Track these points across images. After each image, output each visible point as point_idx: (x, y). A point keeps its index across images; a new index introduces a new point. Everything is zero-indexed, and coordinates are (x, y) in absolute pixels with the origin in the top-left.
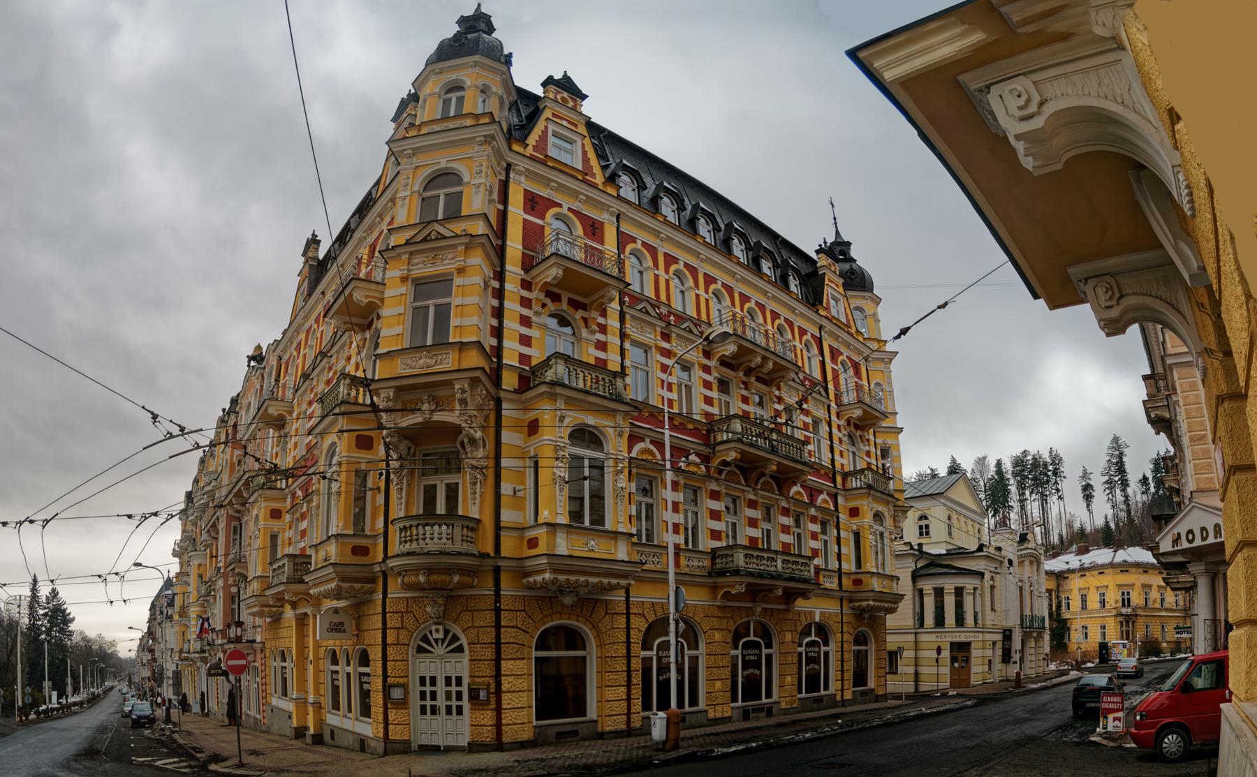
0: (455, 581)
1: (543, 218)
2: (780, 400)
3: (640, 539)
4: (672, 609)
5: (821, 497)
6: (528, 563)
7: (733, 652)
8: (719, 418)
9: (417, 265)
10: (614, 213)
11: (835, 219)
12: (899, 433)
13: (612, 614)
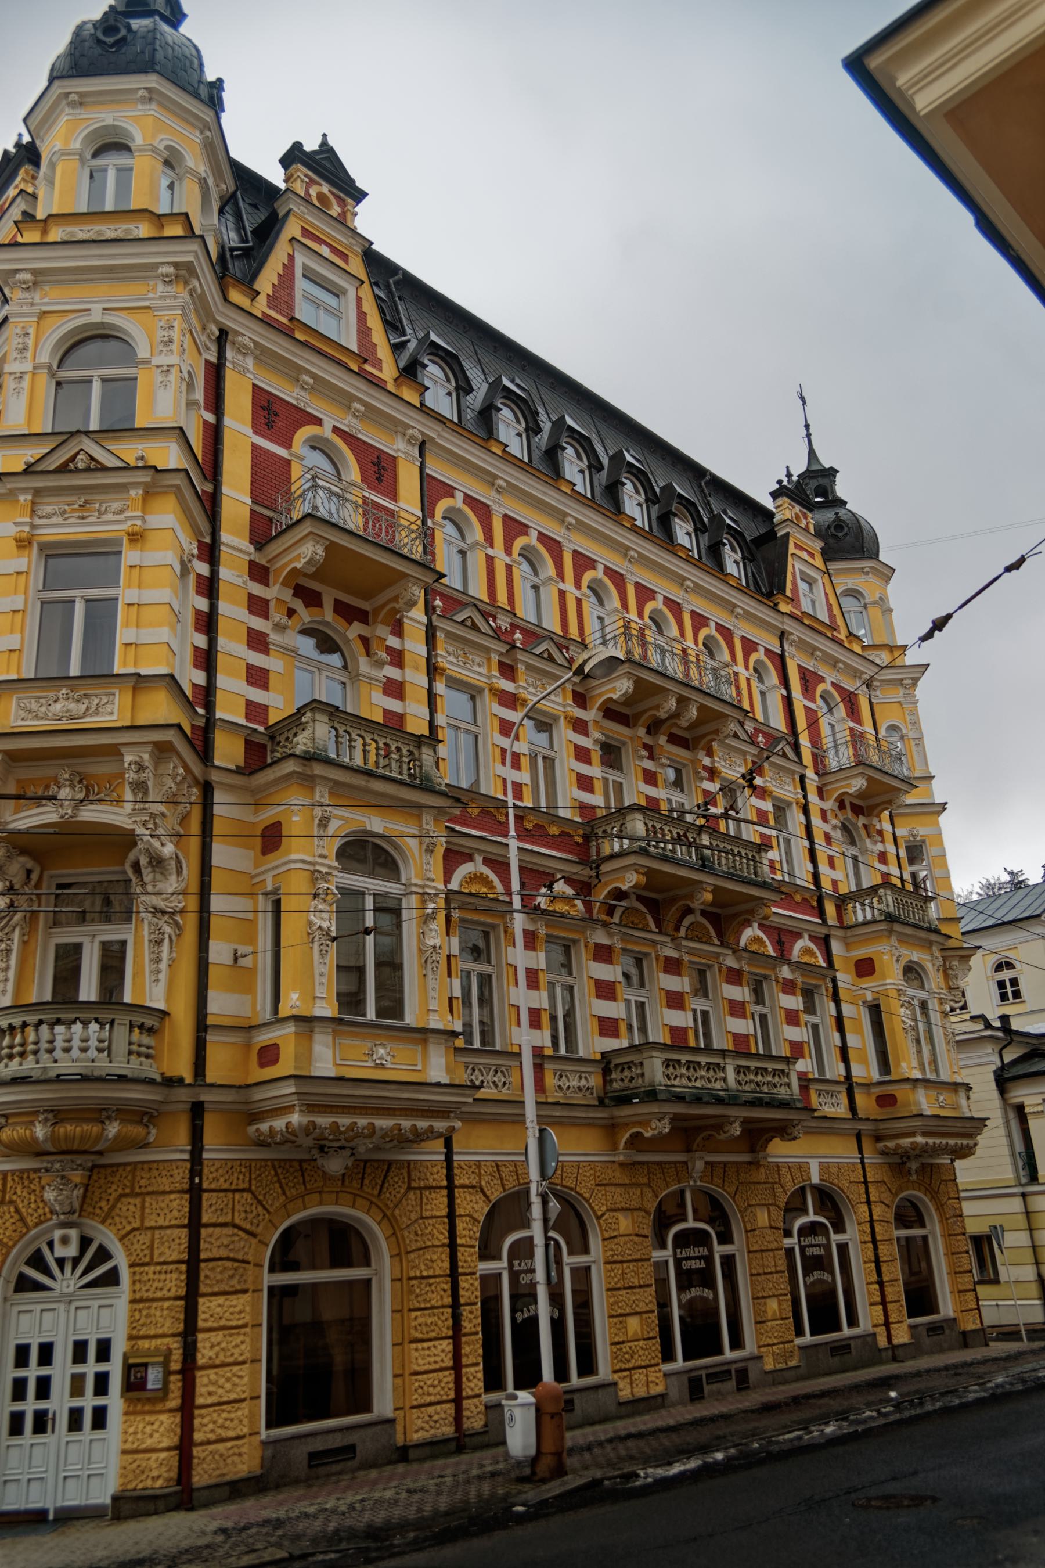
0: (110, 1136)
1: (288, 445)
2: (712, 773)
3: (469, 1041)
4: (534, 1174)
5: (799, 945)
6: (258, 1095)
7: (658, 1255)
8: (604, 812)
9: (49, 516)
10: (416, 439)
11: (807, 426)
12: (939, 813)
13: (419, 1188)
